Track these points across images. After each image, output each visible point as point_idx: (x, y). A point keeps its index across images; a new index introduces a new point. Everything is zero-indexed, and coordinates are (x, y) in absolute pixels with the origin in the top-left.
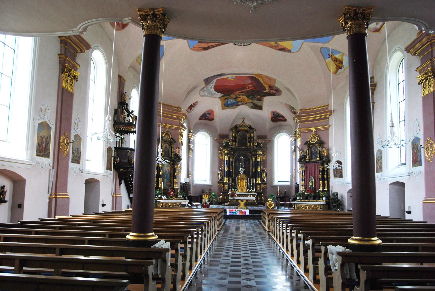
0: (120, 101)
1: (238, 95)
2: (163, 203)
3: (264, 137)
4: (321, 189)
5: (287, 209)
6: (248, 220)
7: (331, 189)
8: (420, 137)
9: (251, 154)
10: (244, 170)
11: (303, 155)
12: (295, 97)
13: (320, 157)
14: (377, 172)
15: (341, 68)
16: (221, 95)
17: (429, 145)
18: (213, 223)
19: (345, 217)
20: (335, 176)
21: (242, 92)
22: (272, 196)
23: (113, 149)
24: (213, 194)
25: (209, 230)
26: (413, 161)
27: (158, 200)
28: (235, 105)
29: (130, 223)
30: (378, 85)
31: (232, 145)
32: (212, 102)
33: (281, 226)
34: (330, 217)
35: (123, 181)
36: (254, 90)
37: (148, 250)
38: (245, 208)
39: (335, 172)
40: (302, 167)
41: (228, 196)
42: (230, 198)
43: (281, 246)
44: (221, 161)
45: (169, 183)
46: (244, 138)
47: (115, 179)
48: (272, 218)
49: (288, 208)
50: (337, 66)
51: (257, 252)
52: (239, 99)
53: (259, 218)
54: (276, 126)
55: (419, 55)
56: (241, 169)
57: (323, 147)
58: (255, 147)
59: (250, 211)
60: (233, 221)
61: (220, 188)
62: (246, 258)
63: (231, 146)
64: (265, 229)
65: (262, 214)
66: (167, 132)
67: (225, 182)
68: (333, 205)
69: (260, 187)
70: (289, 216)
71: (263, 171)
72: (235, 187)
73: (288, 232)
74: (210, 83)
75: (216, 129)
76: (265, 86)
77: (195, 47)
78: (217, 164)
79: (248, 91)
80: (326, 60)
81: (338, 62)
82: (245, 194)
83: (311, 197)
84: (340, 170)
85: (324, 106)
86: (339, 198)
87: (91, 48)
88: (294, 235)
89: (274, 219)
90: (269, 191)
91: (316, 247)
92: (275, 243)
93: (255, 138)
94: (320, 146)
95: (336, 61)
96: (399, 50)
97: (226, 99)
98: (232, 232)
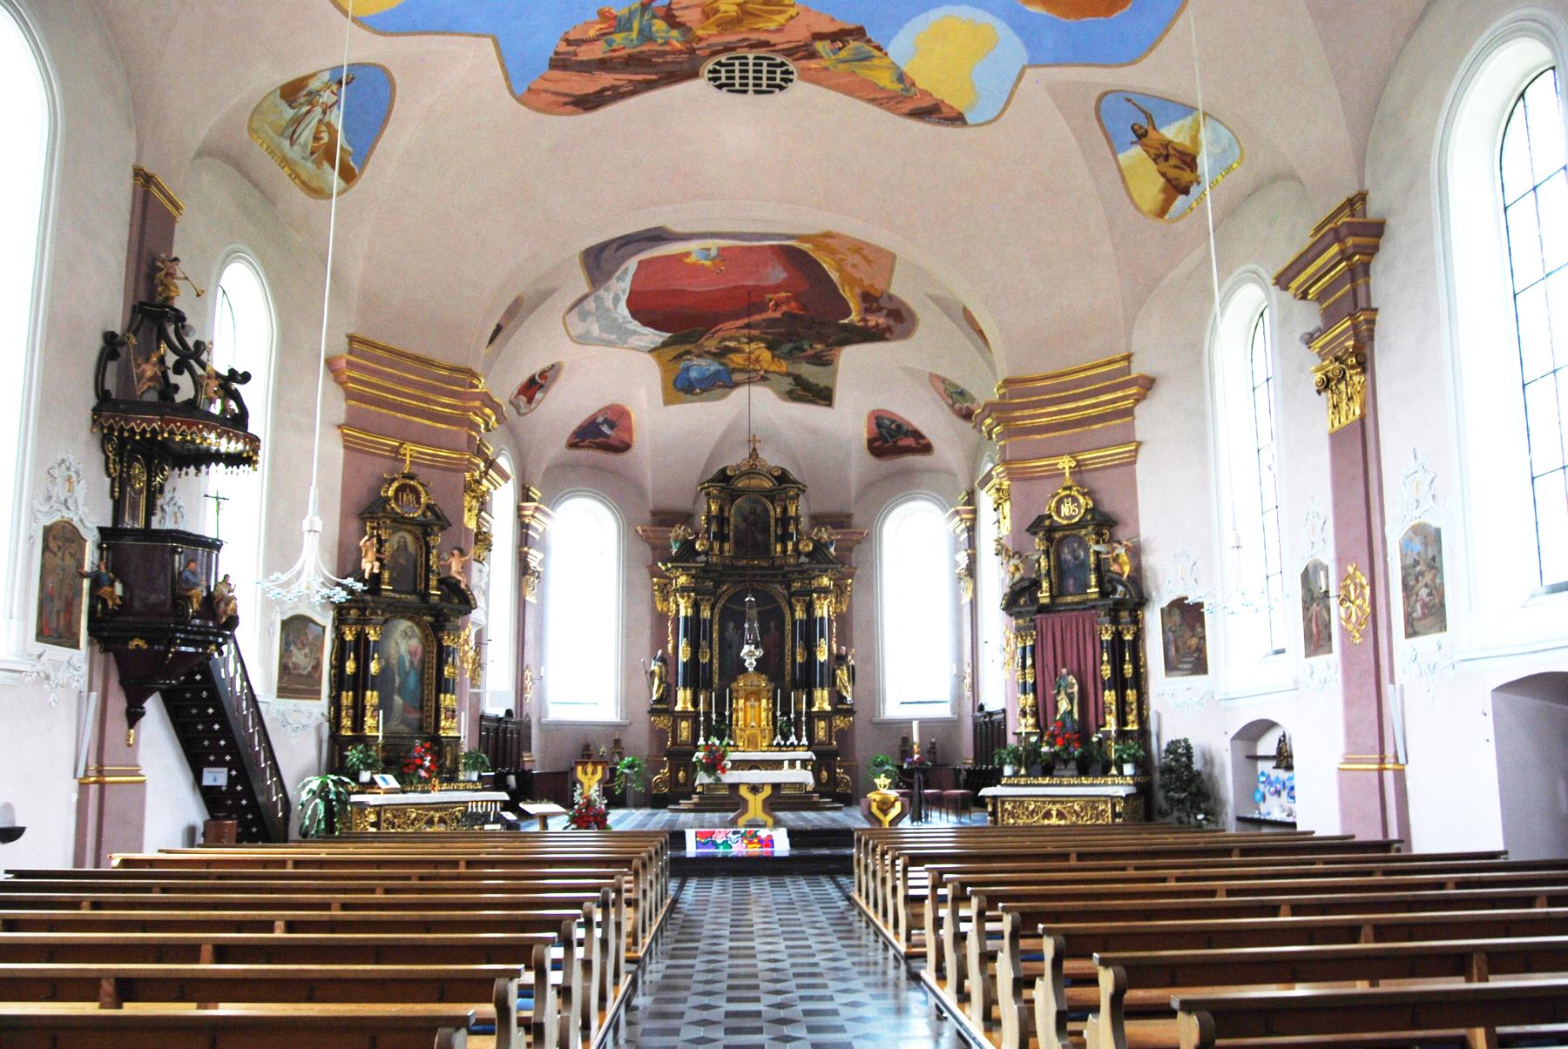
0: (143, 297)
1: (731, 339)
2: (379, 809)
3: (840, 521)
4: (1111, 725)
6: (788, 880)
9: (788, 587)
10: (759, 653)
11: (1022, 579)
13: (1100, 583)
14: (1411, 632)
15: (1186, 191)
17: (1352, 588)
20: (1170, 667)
21: (748, 326)
22: (882, 764)
23: (91, 538)
24: (627, 760)
27: (354, 798)
28: (718, 384)
30: (1392, 223)
31: (706, 553)
32: (617, 368)
33: (899, 875)
35: (153, 707)
38: (770, 821)
39: (1173, 650)
41: (692, 769)
42: (702, 778)
44: (660, 619)
45: (414, 716)
50: (1169, 180)
52: (738, 359)
54: (887, 477)
55: (1320, 298)
56: (746, 648)
57: (1112, 540)
58: (803, 559)
59: (792, 834)
60: (716, 884)
61: (658, 735)
67: (678, 708)
69: (830, 726)
71: (840, 659)
72: (722, 728)
74: (608, 276)
75: (639, 489)
76: (846, 293)
79: (772, 322)
80: (1120, 157)
81: (1173, 161)
83: (1066, 762)
85: (1110, 363)
86: (1197, 765)
90: (864, 747)
92: (881, 939)
94: (1100, 534)
95: (1167, 158)
97: (678, 357)
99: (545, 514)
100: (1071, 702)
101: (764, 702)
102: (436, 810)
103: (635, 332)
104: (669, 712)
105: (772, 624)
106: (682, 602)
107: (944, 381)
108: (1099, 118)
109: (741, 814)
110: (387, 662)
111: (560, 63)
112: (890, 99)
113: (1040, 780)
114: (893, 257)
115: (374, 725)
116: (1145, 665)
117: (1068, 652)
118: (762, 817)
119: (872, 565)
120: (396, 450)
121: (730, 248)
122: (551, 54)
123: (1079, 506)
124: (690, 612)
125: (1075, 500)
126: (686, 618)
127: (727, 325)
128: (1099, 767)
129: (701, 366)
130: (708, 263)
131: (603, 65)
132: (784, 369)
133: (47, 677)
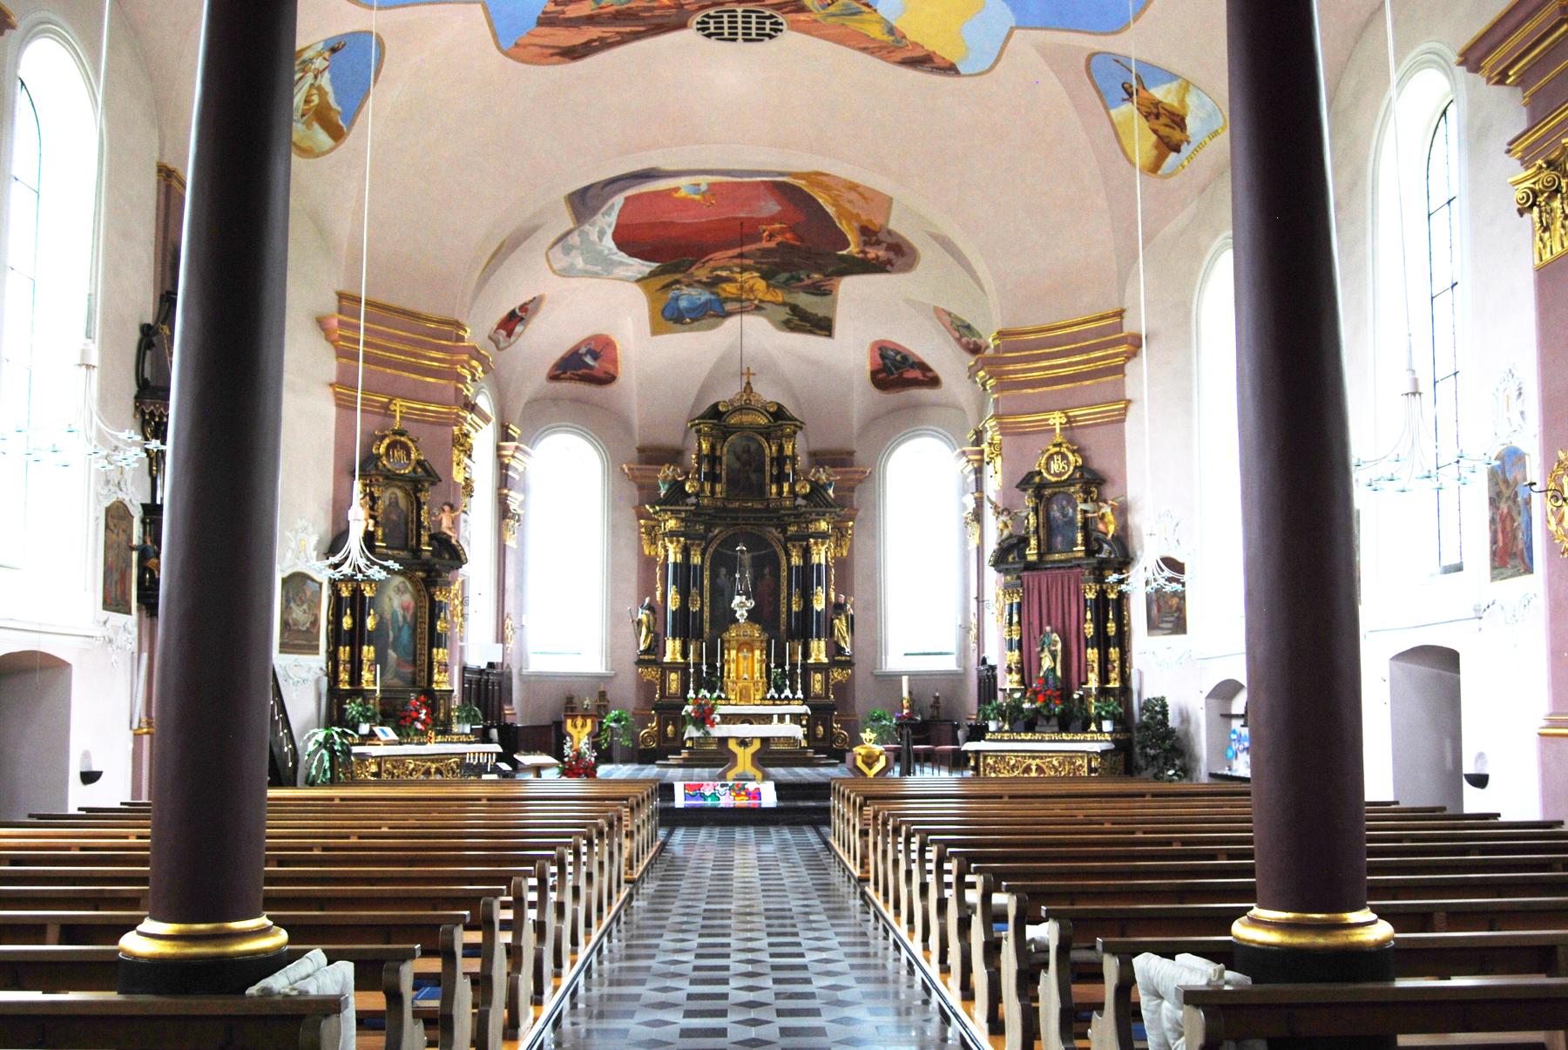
1: (722, 269)
2: (380, 760)
3: (839, 459)
4: (1093, 682)
5: (944, 774)
6: (772, 829)
7: (1135, 685)
8: (1524, 448)
9: (784, 531)
10: (751, 604)
11: (1011, 536)
12: (977, 281)
13: (1086, 542)
15: (1177, 149)
16: (646, 267)
18: (601, 849)
19: (1199, 808)
20: (1153, 626)
21: (741, 256)
22: (879, 719)
23: (137, 514)
24: (614, 713)
25: (582, 883)
26: (1494, 554)
27: (355, 749)
28: (712, 313)
29: (143, 861)
31: (697, 495)
32: (605, 299)
34: (1137, 808)
36: (793, 247)
37: (232, 1011)
38: (759, 775)
40: (1008, 589)
41: (681, 722)
42: (691, 732)
43: (916, 946)
44: (648, 564)
45: (408, 670)
46: (750, 461)
47: (145, 656)
48: (875, 818)
49: (950, 772)
50: (1160, 137)
51: (808, 981)
52: (731, 289)
53: (820, 819)
54: (891, 412)
55: (1522, 82)
56: (737, 599)
57: (1101, 499)
58: (800, 501)
59: (780, 787)
60: (703, 833)
61: (646, 688)
62: (753, 1014)
63: (693, 500)
64: (845, 869)
65: (834, 802)
66: (395, 433)
67: (667, 659)
68: (1146, 755)
69: (827, 678)
70: (952, 806)
71: (839, 608)
72: (713, 680)
73: (949, 885)
74: (594, 211)
76: (843, 226)
77: (525, 46)
78: (634, 579)
79: (766, 252)
80: (1113, 112)
81: (1163, 120)
82: (755, 712)
83: (1048, 719)
84: (1175, 601)
85: (1102, 318)
86: (1173, 722)
87: (13, 27)
88: (973, 897)
89: (885, 823)
90: (864, 700)
91: (1077, 955)
93: (802, 460)
94: (1087, 492)
95: (1157, 116)
96: (1430, 64)
97: (667, 287)
98: (697, 886)
99: (525, 453)
100: (1054, 660)
101: (757, 653)
102: (433, 761)
103: (621, 263)
104: (657, 663)
105: (766, 571)
106: (671, 548)
107: (949, 314)
108: (1090, 77)
109: (730, 768)
110: (381, 617)
111: (546, 21)
112: (881, 48)
113: (1023, 736)
114: (891, 199)
115: (370, 679)
116: (1129, 624)
117: (1053, 607)
118: (751, 771)
119: (875, 506)
120: (386, 407)
121: (720, 184)
122: (539, 13)
123: (1068, 464)
124: (679, 557)
125: (1064, 457)
126: (675, 564)
127: (718, 255)
128: (1079, 723)
129: (691, 296)
130: (697, 197)
131: (591, 20)
132: (780, 299)
133: (110, 641)
